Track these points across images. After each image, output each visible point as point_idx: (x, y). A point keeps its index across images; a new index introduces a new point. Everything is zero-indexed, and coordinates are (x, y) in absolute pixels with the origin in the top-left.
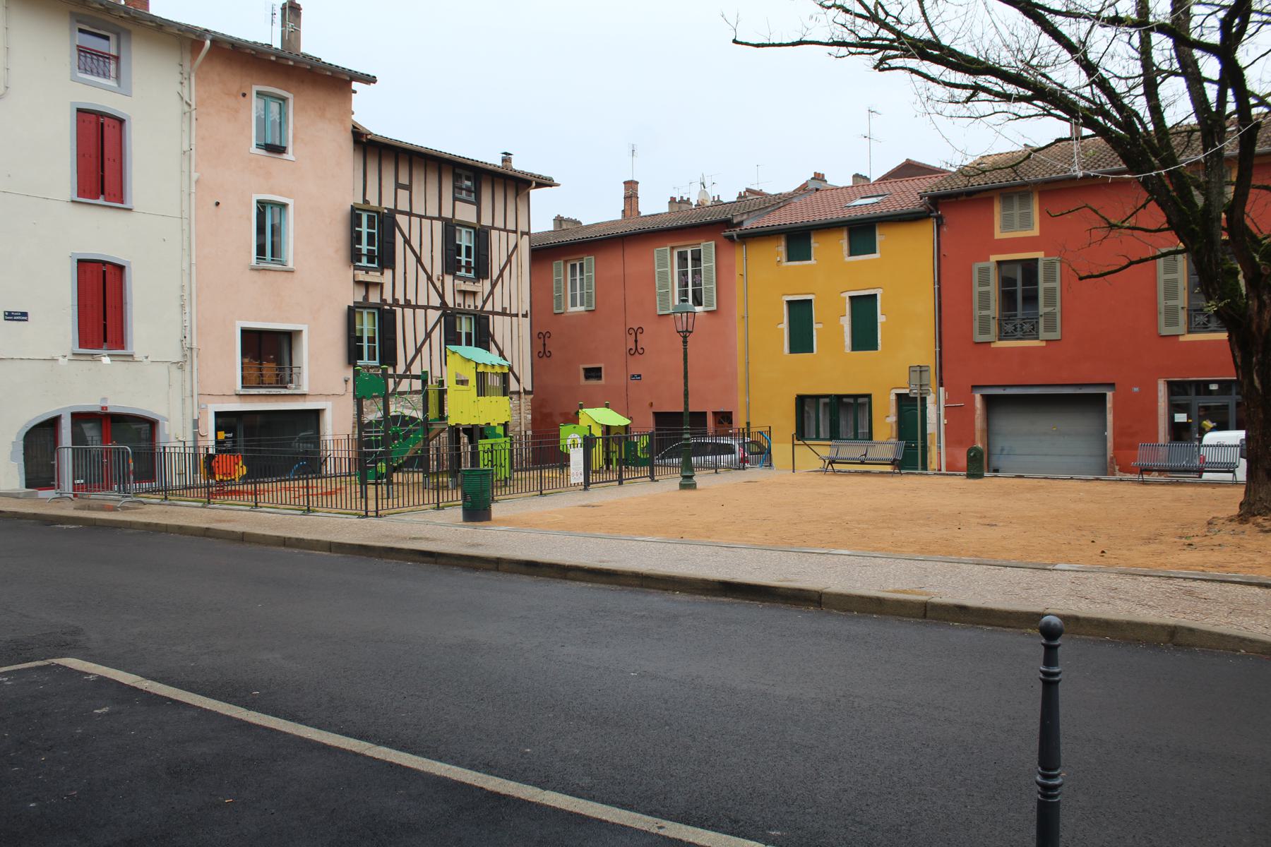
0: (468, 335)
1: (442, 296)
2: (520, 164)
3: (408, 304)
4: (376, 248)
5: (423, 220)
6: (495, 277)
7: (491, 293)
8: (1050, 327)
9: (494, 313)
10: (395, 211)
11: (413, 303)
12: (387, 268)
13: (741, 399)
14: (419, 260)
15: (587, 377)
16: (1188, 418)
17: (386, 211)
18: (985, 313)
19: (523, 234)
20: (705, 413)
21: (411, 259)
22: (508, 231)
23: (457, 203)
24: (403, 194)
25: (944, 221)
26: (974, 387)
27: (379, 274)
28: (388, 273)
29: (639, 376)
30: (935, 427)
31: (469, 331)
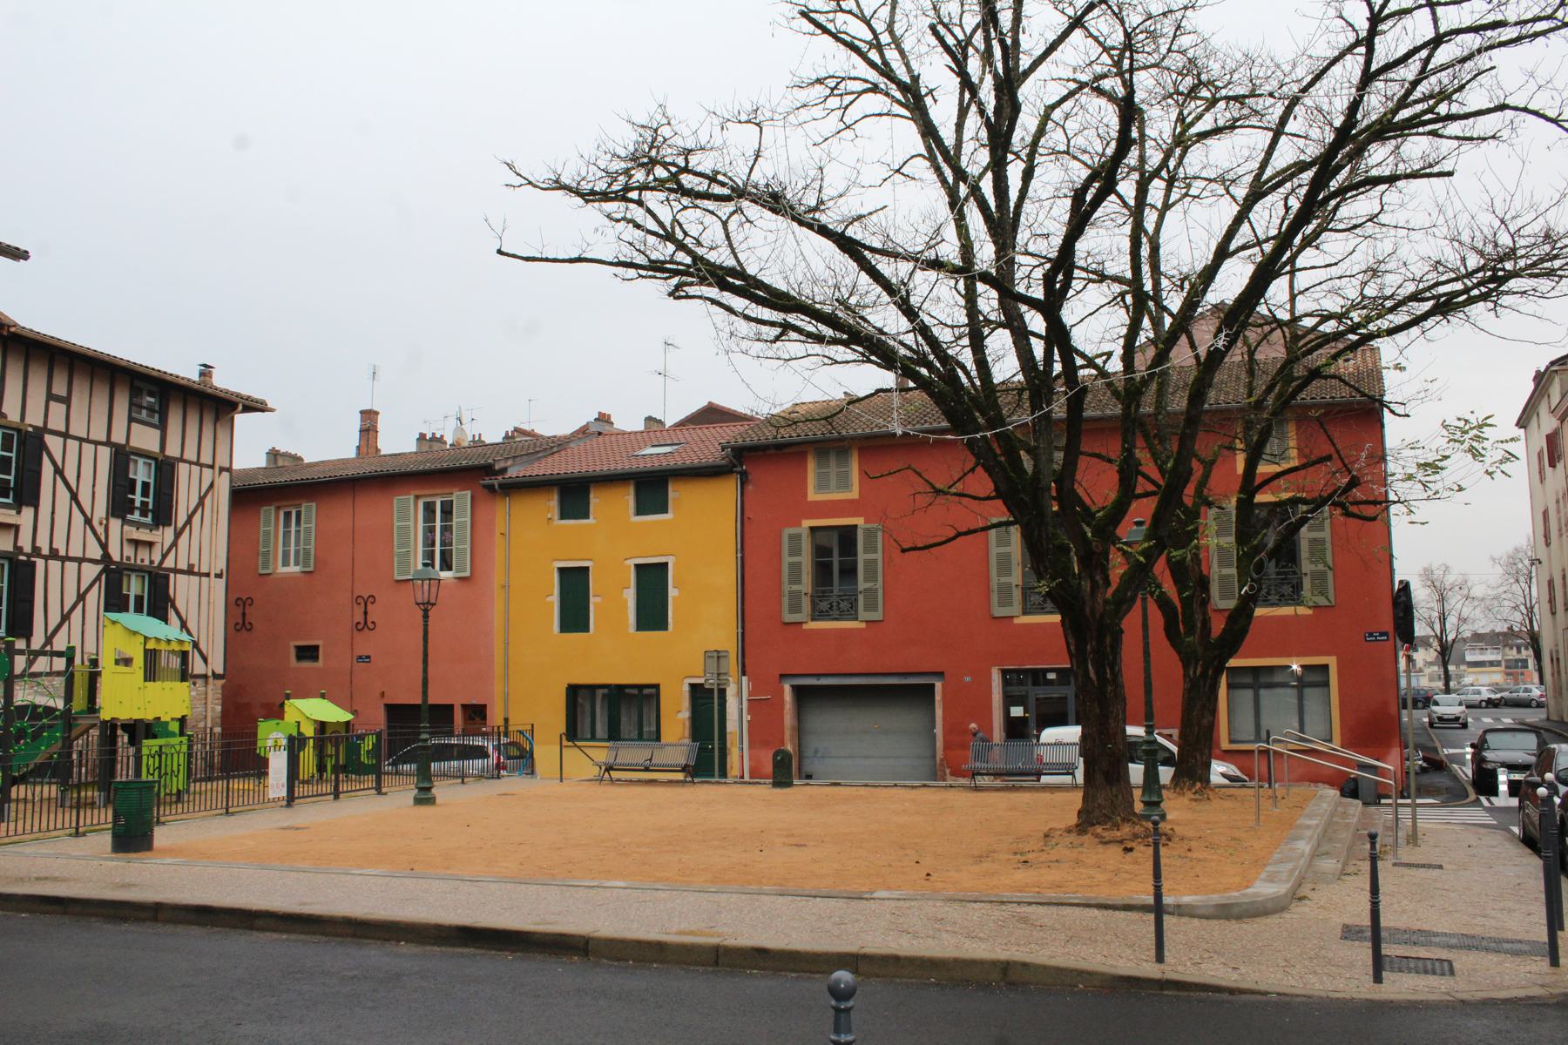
0: (139, 599)
1: (104, 546)
2: (223, 381)
3: (54, 554)
4: (12, 478)
5: (84, 444)
6: (180, 524)
7: (175, 544)
8: (870, 606)
9: (176, 571)
10: (44, 430)
11: (62, 553)
12: (27, 505)
13: (498, 689)
14: (74, 497)
15: (299, 658)
16: (1025, 712)
17: (30, 429)
18: (795, 587)
19: (222, 470)
20: (450, 708)
21: (63, 495)
22: (202, 466)
23: (134, 425)
24: (57, 410)
25: (750, 477)
26: (783, 676)
27: (14, 512)
28: (28, 512)
29: (369, 657)
30: (737, 724)
31: (139, 593)
